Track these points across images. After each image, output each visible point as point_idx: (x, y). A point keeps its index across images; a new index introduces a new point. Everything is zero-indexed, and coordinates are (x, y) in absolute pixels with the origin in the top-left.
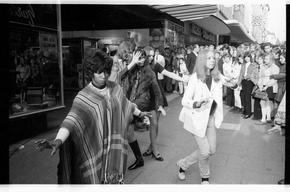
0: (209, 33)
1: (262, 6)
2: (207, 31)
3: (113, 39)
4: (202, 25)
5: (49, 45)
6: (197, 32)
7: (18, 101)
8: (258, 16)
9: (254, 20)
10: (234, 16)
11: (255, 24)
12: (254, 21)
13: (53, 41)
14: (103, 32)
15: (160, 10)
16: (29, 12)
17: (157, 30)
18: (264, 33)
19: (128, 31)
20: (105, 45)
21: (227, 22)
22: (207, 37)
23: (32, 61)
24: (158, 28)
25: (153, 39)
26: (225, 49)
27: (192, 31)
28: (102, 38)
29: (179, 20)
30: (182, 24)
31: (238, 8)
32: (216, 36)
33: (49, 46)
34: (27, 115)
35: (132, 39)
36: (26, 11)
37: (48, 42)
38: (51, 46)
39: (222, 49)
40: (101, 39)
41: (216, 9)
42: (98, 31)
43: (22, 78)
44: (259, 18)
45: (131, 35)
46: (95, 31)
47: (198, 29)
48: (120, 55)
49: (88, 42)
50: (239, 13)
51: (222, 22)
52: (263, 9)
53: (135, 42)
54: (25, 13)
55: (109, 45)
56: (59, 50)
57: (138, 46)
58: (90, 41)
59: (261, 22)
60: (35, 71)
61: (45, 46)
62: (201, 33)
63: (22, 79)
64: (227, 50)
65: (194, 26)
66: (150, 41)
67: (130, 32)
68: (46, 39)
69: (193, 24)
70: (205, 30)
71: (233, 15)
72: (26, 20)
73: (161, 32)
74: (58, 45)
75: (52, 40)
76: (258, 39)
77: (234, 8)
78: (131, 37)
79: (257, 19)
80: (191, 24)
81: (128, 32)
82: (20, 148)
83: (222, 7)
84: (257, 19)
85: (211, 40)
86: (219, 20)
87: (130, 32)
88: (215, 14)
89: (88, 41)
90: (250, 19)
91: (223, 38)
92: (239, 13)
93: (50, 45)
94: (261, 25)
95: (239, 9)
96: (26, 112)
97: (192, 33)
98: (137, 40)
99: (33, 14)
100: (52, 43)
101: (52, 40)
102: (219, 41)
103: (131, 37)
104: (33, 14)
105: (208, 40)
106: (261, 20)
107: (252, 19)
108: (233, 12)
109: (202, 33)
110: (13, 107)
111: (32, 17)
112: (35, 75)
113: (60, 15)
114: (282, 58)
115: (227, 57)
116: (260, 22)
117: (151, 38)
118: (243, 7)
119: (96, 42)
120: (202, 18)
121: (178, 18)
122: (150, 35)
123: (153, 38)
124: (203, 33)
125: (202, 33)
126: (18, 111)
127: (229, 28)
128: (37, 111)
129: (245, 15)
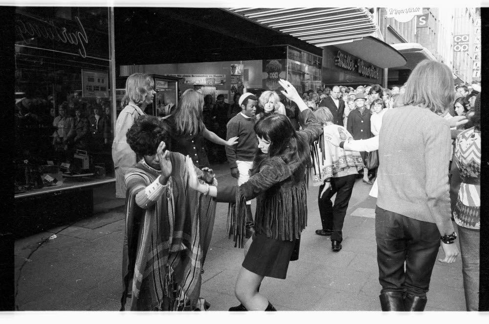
0: (369, 65)
1: (471, 18)
2: (365, 62)
3: (208, 77)
4: (357, 52)
5: (97, 88)
6: (347, 64)
7: (52, 171)
8: (462, 36)
9: (455, 42)
10: (417, 36)
11: (457, 48)
12: (456, 44)
13: (103, 82)
14: (186, 65)
15: (280, 30)
16: (80, 34)
17: (275, 62)
18: (475, 63)
19: (232, 63)
20: (195, 85)
21: (399, 46)
22: (366, 72)
23: (77, 113)
24: (278, 59)
25: (269, 77)
26: (374, 92)
27: (338, 62)
28: (191, 75)
29: (312, 45)
30: (319, 51)
31: (424, 22)
32: (383, 70)
33: (97, 90)
34: (61, 190)
35: (238, 77)
36: (75, 33)
37: (96, 83)
38: (98, 90)
39: (370, 93)
40: (190, 76)
41: (372, 27)
42: (185, 64)
43: (61, 136)
44: (465, 38)
45: (237, 70)
46: (180, 65)
47: (349, 58)
48: (134, 101)
49: (162, 83)
50: (428, 31)
51: (388, 48)
52: (473, 22)
53: (243, 81)
54: (72, 36)
55: (204, 86)
56: (110, 93)
57: (248, 87)
58: (165, 81)
59: (468, 45)
60: (82, 128)
61: (90, 90)
62: (354, 66)
63: (62, 138)
64: (378, 94)
65: (342, 55)
66: (264, 80)
67: (235, 65)
68: (91, 79)
69: (339, 52)
70: (361, 61)
71: (415, 35)
72: (75, 48)
73: (281, 66)
74: (110, 86)
75: (101, 81)
76: (465, 74)
77: (418, 24)
78: (236, 73)
79: (460, 40)
80: (335, 51)
81: (232, 65)
82: (50, 239)
83: (394, 22)
84: (460, 40)
85: (373, 76)
86: (382, 45)
87: (235, 65)
88: (374, 35)
89: (163, 81)
90: (449, 40)
91: (398, 72)
92: (428, 31)
93: (98, 87)
94: (467, 50)
95: (426, 23)
96: (61, 186)
97: (337, 66)
98: (246, 78)
99: (85, 38)
100: (100, 84)
101: (101, 81)
102: (388, 79)
103: (236, 73)
104: (85, 38)
105: (368, 77)
106: (468, 41)
107: (452, 41)
108: (415, 29)
109: (356, 66)
110: (43, 180)
111: (84, 42)
112: (83, 133)
113: (114, 47)
114: (458, 107)
115: (379, 104)
116: (466, 46)
117: (266, 75)
118: (436, 20)
119: (175, 82)
120: (352, 41)
121: (310, 42)
122: (264, 71)
123: (269, 74)
124: (358, 66)
125: (356, 66)
126: (49, 184)
127: (404, 57)
128: (77, 184)
129: (439, 35)
